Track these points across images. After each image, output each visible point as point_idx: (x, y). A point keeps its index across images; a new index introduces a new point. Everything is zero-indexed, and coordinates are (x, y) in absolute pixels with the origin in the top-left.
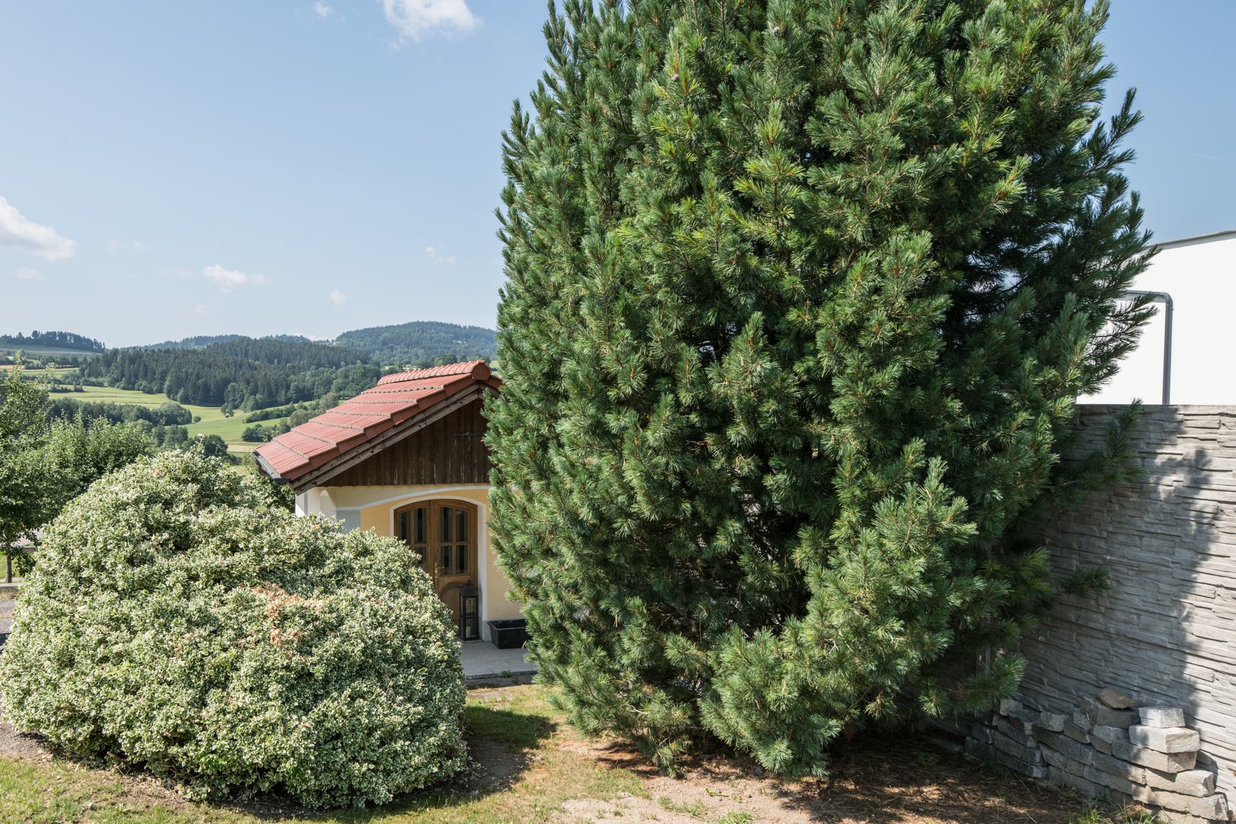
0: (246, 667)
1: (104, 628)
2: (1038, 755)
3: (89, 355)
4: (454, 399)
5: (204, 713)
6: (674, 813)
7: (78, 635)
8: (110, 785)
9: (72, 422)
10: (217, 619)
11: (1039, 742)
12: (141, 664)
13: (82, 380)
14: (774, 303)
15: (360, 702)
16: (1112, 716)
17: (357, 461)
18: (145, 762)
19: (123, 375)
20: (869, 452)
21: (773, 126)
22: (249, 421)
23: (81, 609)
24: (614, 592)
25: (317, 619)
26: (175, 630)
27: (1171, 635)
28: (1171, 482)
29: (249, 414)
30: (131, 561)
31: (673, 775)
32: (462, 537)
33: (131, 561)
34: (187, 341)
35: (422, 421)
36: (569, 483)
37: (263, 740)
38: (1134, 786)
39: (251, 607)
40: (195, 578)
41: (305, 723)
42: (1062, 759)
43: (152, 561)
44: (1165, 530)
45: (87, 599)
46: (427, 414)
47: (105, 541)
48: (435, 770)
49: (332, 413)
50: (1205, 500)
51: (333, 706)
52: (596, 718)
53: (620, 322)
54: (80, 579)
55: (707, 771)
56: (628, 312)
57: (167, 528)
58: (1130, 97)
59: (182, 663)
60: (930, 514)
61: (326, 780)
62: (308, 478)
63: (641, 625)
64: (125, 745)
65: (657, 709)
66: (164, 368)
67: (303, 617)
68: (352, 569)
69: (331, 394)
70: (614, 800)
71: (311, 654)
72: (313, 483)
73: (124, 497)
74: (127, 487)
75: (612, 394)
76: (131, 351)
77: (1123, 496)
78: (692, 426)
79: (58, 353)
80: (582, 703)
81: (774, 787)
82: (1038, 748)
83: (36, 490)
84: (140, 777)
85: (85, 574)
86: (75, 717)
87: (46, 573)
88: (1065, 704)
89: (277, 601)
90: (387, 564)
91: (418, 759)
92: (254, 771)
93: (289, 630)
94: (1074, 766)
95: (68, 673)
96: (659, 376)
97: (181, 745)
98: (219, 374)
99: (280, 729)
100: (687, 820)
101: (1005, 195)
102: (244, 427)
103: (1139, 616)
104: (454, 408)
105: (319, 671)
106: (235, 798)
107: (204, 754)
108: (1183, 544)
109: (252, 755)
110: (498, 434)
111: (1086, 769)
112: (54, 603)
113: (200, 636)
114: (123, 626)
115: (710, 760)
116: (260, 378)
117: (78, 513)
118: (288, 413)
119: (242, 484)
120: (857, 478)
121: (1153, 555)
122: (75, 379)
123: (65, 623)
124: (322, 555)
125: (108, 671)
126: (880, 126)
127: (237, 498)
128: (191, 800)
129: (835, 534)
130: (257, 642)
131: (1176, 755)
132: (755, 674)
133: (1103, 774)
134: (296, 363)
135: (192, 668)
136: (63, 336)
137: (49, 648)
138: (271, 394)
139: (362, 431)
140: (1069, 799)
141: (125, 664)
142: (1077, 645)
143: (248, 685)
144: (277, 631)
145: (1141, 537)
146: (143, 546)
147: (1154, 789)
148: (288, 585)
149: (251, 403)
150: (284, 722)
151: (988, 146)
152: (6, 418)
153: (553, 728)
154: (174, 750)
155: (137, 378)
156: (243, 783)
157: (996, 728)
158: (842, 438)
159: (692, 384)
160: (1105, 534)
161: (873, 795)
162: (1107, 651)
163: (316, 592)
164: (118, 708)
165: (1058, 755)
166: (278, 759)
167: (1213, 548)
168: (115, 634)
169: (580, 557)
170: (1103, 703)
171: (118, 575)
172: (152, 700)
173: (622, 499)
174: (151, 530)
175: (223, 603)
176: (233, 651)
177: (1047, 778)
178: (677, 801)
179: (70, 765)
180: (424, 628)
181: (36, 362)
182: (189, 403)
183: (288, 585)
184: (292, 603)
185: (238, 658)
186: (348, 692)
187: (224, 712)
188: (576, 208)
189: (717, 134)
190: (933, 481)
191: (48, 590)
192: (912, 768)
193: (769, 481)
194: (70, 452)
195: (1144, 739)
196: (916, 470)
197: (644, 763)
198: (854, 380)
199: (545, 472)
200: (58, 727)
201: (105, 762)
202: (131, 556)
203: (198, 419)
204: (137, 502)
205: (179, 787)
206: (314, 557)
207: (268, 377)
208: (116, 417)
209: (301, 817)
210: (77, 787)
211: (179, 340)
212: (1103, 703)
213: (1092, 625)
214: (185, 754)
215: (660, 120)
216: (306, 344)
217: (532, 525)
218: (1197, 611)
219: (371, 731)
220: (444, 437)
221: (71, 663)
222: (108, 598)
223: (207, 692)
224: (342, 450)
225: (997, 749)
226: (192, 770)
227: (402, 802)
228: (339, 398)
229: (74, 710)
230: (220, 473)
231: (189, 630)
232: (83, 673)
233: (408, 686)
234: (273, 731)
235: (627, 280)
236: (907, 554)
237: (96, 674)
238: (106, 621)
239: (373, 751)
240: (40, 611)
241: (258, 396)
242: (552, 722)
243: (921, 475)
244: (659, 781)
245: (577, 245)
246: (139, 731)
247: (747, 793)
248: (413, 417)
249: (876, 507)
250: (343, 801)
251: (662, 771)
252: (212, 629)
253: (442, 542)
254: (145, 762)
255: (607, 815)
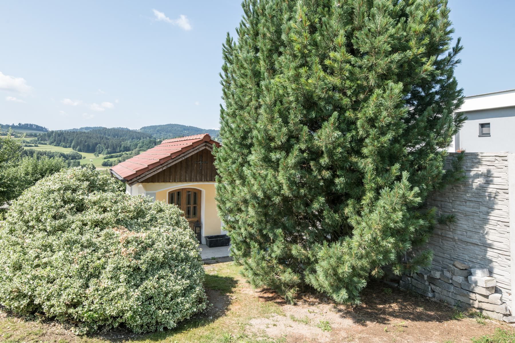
0: (109, 267)
1: (39, 251)
2: (430, 288)
3: (42, 133)
4: (196, 148)
5: (87, 291)
6: (297, 322)
7: (25, 254)
8: (36, 330)
9: (32, 157)
10: (96, 244)
11: (430, 283)
12: (57, 268)
13: (38, 142)
14: (342, 110)
15: (162, 281)
16: (460, 272)
17: (156, 173)
18: (55, 316)
19: (55, 141)
20: (377, 169)
21: (341, 39)
22: (105, 158)
23: (27, 241)
24: (269, 226)
25: (143, 242)
26: (75, 250)
27: (480, 240)
28: (478, 182)
29: (105, 156)
30: (54, 217)
31: (292, 304)
32: (195, 203)
33: (54, 217)
34: (82, 128)
35: (183, 157)
36: (253, 181)
37: (116, 303)
38: (471, 301)
39: (112, 238)
40: (85, 225)
41: (136, 293)
42: (440, 289)
43: (65, 217)
44: (475, 199)
45: (31, 236)
46: (185, 154)
47: (42, 208)
48: (195, 310)
49: (136, 158)
50: (491, 189)
51: (150, 283)
52: (262, 281)
53: (276, 115)
54: (28, 227)
55: (305, 301)
56: (280, 112)
57: (73, 201)
58: (459, 40)
59: (77, 266)
60: (404, 194)
61: (146, 320)
62: (135, 179)
63: (281, 241)
64: (45, 309)
65: (287, 276)
66: (72, 138)
67: (136, 241)
68: (156, 218)
69: (137, 149)
70: (271, 318)
71: (140, 259)
72: (137, 181)
73: (53, 187)
74: (54, 183)
75: (272, 144)
76: (59, 132)
77: (458, 186)
78: (305, 158)
79: (29, 132)
80: (256, 274)
81: (335, 308)
82: (430, 285)
83: (13, 184)
84: (53, 324)
85: (31, 224)
86: (21, 295)
87: (11, 223)
88: (438, 267)
89: (125, 235)
90: (170, 215)
91: (187, 305)
92: (111, 318)
93: (130, 248)
94: (445, 292)
95: (18, 273)
96: (293, 137)
97: (75, 308)
98: (94, 141)
99: (125, 297)
100: (304, 326)
101: (426, 71)
102: (103, 161)
103: (466, 232)
104: (196, 152)
105: (144, 268)
106: (101, 331)
107: (87, 312)
108: (483, 205)
109: (111, 310)
110: (220, 161)
111: (450, 293)
112: (14, 238)
113: (87, 253)
114: (48, 249)
115: (305, 296)
116: (110, 143)
117: (29, 195)
118: (120, 156)
119: (109, 181)
120: (373, 179)
121: (471, 209)
122: (35, 142)
123: (18, 248)
124: (143, 212)
125: (40, 272)
126: (382, 42)
127: (106, 188)
128: (78, 335)
129: (363, 202)
130: (115, 255)
131: (488, 288)
132: (333, 261)
133: (458, 296)
134: (124, 138)
135: (82, 268)
136: (31, 125)
137: (9, 261)
138: (114, 149)
139: (158, 160)
140: (446, 306)
141: (49, 268)
142: (442, 244)
143: (110, 276)
144: (125, 249)
145: (466, 202)
146: (61, 210)
147: (479, 302)
148: (129, 227)
149: (106, 152)
150: (127, 293)
151: (420, 52)
152: (2, 154)
153: (236, 282)
154: (71, 311)
155: (61, 142)
156: (105, 324)
157: (412, 277)
158: (367, 165)
159: (306, 141)
160: (451, 201)
161: (374, 309)
162: (454, 246)
163: (142, 230)
164: (42, 291)
165: (438, 288)
166: (123, 312)
167: (496, 207)
168: (44, 254)
169: (257, 213)
170: (456, 267)
171: (47, 224)
172: (61, 286)
173: (276, 188)
174: (65, 202)
175: (99, 236)
176: (103, 260)
177: (434, 297)
178: (297, 316)
179: (15, 319)
180: (187, 243)
181: (19, 135)
182: (81, 152)
183: (129, 227)
184: (131, 235)
185: (106, 263)
186: (156, 276)
187: (97, 290)
188: (257, 70)
189: (315, 44)
190: (404, 180)
191: (11, 231)
192: (383, 295)
193: (337, 181)
194: (30, 169)
195: (476, 283)
196: (397, 176)
197: (279, 298)
198: (373, 140)
199: (242, 177)
200: (10, 301)
201: (35, 317)
202: (55, 215)
203: (85, 158)
204: (59, 190)
205: (72, 329)
206: (140, 213)
207: (113, 143)
208: (51, 156)
209: (133, 339)
210: (18, 333)
211: (78, 128)
212: (456, 267)
213: (447, 236)
214: (77, 312)
215: (293, 36)
216: (128, 131)
217: (235, 199)
218: (491, 230)
219: (166, 294)
220: (196, 162)
221: (20, 268)
222: (42, 235)
223: (89, 280)
224: (150, 168)
225: (413, 286)
226: (79, 320)
227: (181, 326)
228: (140, 150)
229: (20, 292)
230: (99, 177)
231: (82, 250)
232: (26, 273)
233: (183, 272)
234: (121, 298)
235: (279, 100)
236: (394, 210)
237: (33, 273)
238: (40, 246)
239: (168, 303)
240: (6, 243)
241: (109, 149)
242: (235, 279)
243: (399, 178)
244: (287, 307)
245: (258, 85)
246: (53, 302)
247: (325, 311)
248: (179, 155)
249: (380, 191)
250: (153, 328)
251: (287, 302)
252: (93, 249)
253: (190, 205)
254: (55, 316)
255: (270, 326)
